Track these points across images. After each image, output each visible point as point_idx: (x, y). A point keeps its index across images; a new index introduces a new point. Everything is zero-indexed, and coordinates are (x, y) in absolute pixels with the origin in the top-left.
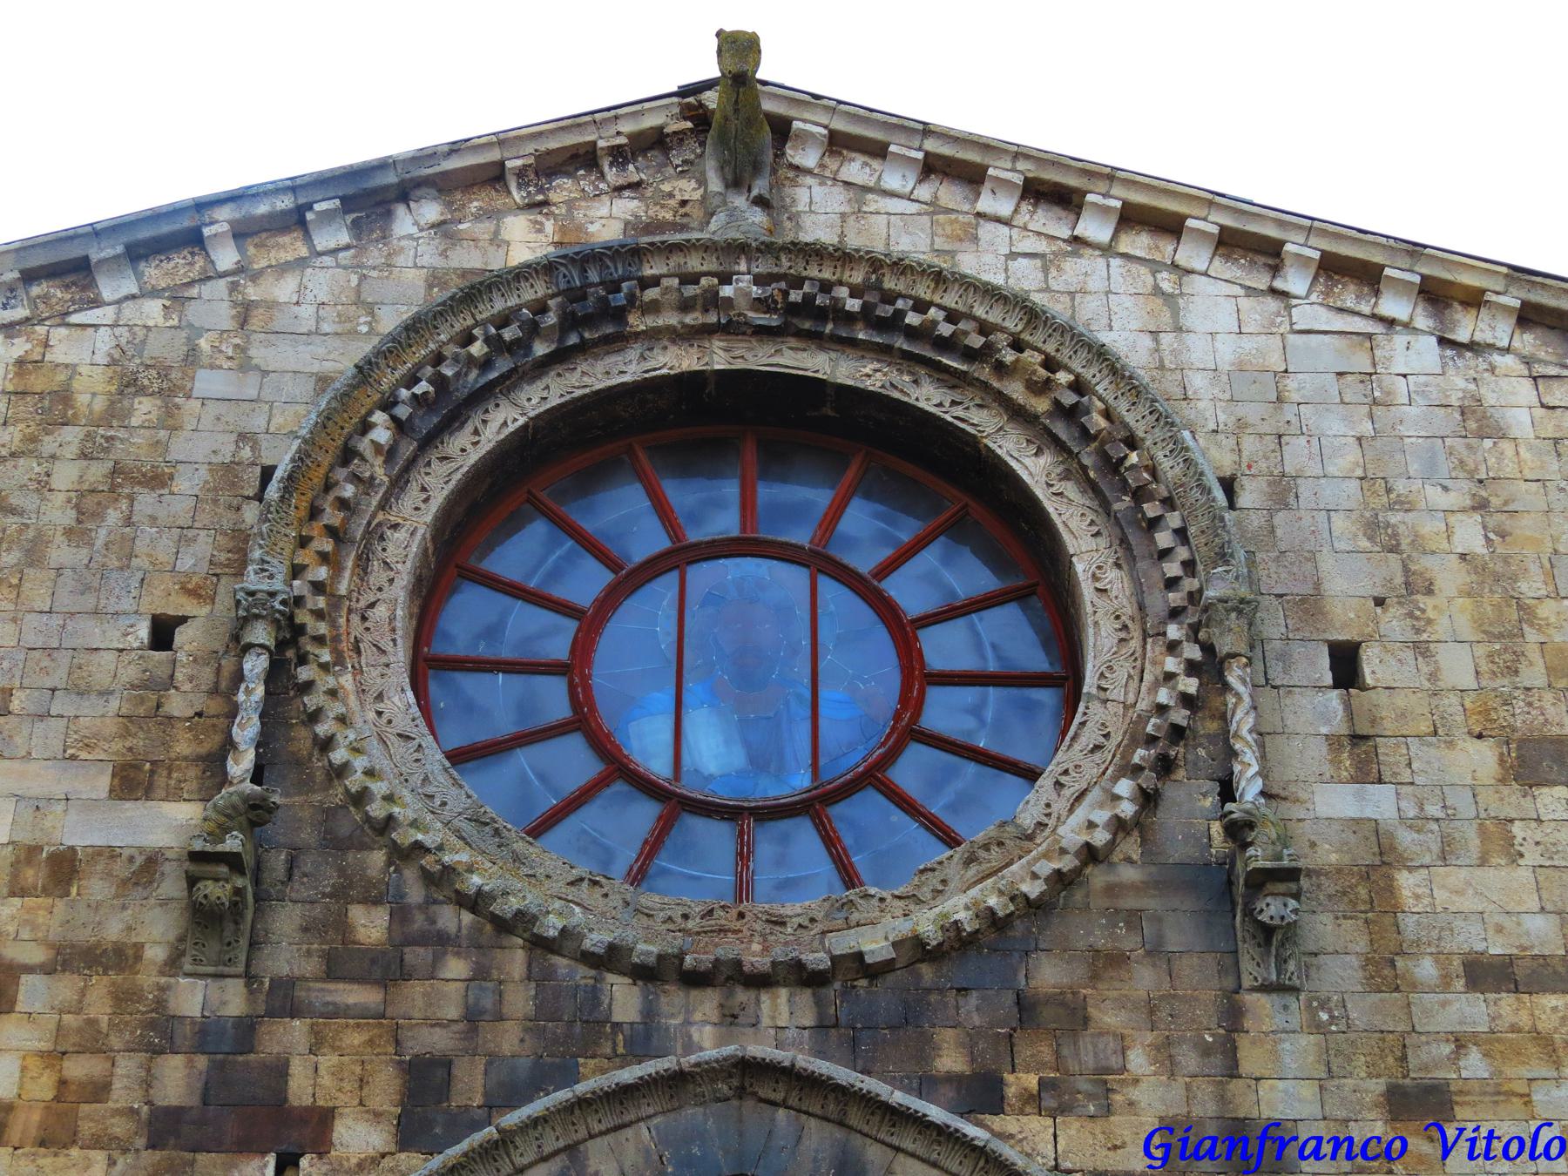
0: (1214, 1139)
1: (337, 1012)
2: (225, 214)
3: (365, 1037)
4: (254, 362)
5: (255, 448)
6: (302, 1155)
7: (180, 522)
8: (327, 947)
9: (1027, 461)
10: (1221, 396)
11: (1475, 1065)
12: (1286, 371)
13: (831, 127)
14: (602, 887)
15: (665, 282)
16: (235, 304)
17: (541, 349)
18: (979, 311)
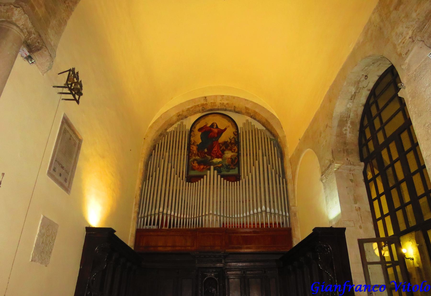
0: (361, 286)
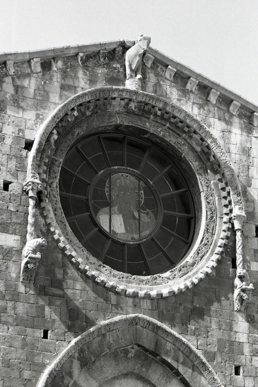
1: (54, 295)
2: (13, 57)
3: (61, 302)
4: (21, 105)
5: (23, 133)
6: (49, 330)
7: (7, 153)
8: (51, 278)
9: (193, 163)
10: (237, 153)
12: (251, 148)
13: (156, 57)
14: (105, 267)
15: (117, 99)
16: (14, 86)
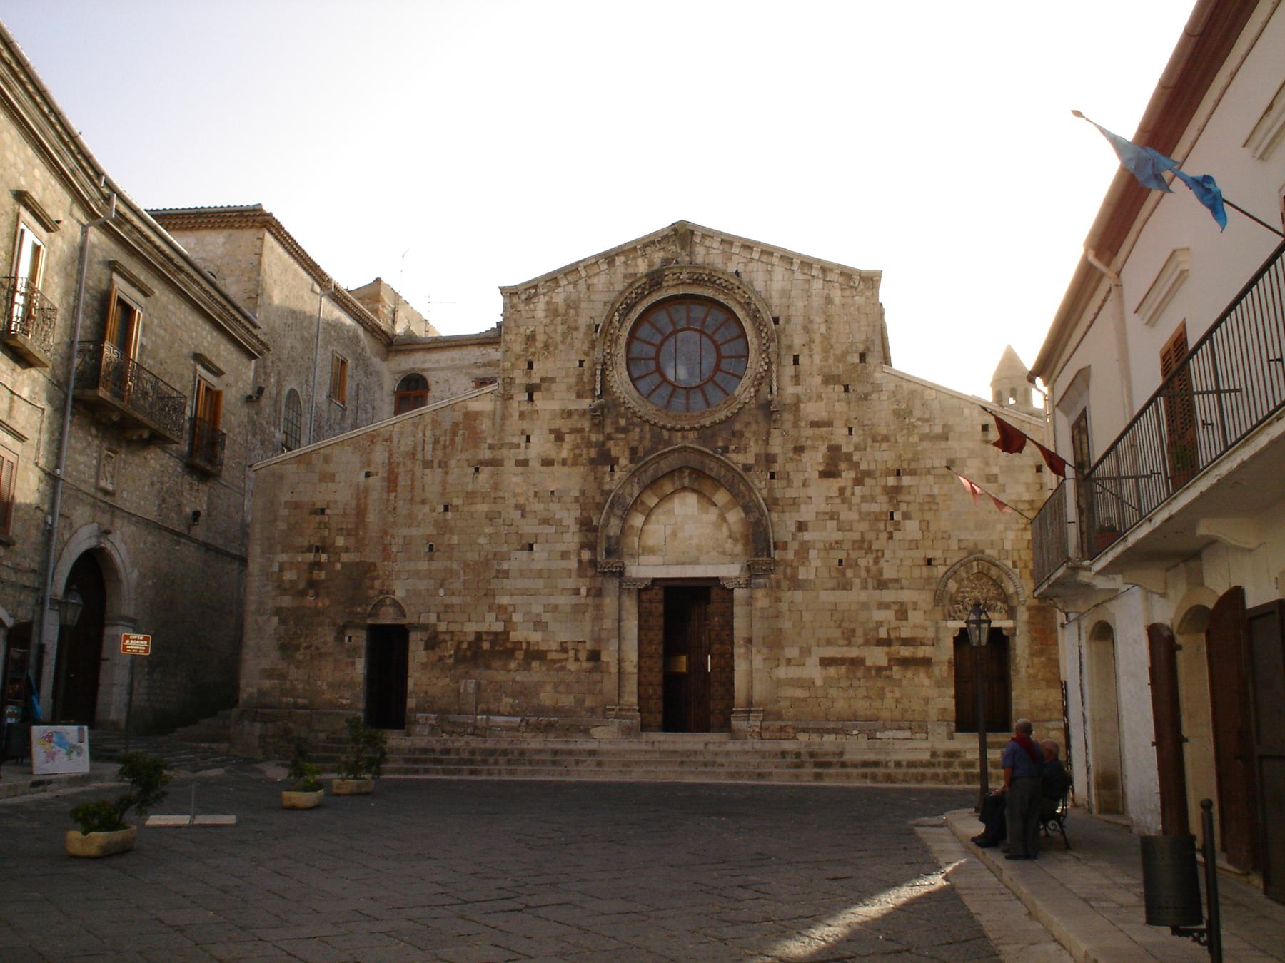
2: (581, 264)
11: (809, 443)
17: (646, 293)
18: (731, 280)
